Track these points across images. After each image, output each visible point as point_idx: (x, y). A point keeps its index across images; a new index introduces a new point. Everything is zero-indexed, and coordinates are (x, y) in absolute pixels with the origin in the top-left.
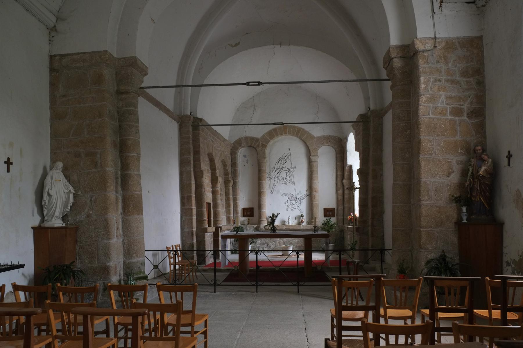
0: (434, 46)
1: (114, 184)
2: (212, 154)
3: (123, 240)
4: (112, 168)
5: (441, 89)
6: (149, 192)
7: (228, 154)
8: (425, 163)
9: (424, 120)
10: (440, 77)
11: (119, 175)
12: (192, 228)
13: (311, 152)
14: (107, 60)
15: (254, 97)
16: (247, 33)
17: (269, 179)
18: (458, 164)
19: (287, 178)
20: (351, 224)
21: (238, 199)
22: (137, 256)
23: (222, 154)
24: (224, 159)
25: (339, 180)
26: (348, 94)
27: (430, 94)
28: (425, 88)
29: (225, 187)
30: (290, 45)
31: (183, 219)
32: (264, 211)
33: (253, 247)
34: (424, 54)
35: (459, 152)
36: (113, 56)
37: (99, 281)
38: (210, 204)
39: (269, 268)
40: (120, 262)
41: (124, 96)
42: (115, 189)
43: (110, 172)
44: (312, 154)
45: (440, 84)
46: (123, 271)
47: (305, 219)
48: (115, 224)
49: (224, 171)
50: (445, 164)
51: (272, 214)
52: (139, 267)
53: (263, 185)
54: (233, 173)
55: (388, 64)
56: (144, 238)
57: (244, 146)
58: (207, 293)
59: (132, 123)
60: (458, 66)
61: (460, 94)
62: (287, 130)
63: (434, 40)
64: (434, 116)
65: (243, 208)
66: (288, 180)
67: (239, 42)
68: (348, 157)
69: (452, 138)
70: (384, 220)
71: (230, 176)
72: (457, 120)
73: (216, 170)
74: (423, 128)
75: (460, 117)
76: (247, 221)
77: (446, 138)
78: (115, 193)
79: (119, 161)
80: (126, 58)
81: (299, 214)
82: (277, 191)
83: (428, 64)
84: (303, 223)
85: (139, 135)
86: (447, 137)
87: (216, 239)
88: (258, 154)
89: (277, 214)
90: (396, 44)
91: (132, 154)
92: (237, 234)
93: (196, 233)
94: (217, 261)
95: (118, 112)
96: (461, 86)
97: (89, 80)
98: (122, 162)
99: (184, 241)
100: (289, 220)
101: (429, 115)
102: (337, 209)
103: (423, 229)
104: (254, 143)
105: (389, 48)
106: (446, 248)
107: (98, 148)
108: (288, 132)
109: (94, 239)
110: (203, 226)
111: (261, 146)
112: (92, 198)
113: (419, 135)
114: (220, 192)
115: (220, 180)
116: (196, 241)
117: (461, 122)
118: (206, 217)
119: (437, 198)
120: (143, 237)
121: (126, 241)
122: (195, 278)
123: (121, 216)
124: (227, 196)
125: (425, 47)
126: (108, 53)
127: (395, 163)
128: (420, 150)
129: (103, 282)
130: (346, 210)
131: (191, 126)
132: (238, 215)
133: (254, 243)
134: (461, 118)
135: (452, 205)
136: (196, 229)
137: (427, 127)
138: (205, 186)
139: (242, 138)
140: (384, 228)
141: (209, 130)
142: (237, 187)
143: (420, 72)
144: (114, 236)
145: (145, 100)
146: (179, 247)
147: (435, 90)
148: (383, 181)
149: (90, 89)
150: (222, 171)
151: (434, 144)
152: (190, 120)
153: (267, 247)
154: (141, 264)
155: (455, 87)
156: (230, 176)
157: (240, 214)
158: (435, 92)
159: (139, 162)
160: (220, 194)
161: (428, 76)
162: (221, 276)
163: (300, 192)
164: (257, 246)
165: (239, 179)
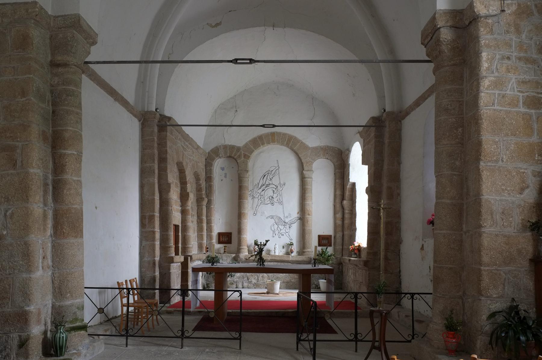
0: (501, 9)
1: (42, 193)
2: (182, 163)
3: (53, 273)
4: (39, 170)
5: (510, 70)
6: (96, 207)
7: (201, 166)
8: (488, 174)
9: (487, 113)
10: (509, 54)
11: (50, 180)
12: (154, 257)
13: (304, 166)
14: (37, 15)
15: (235, 96)
16: (232, 11)
17: (251, 197)
18: (535, 176)
19: (274, 197)
20: (353, 256)
21: (213, 221)
22: (72, 296)
23: (195, 164)
24: (197, 172)
25: (338, 201)
26: (354, 94)
27: (495, 77)
28: (488, 69)
29: (198, 206)
30: (285, 27)
31: (143, 245)
32: (245, 238)
33: (230, 281)
34: (488, 20)
35: (536, 159)
36: (46, 13)
37: (12, 333)
38: (178, 226)
39: (253, 311)
40: (46, 305)
41: (60, 70)
42: (42, 200)
43: (35, 174)
44: (306, 168)
45: (510, 62)
46: (51, 318)
47: (295, 248)
48: (41, 250)
49: (197, 186)
50: (516, 176)
51: (255, 241)
52: (75, 313)
53: (245, 204)
54: (208, 189)
55: (430, 38)
56: (83, 272)
57: (222, 156)
58: (171, 347)
59: (71, 108)
60: (533, 39)
61: (537, 78)
62: (276, 139)
63: (501, 2)
64: (500, 108)
65: (219, 233)
66: (275, 200)
67: (221, 22)
68: (350, 173)
69: (526, 139)
70: (401, 252)
71: (204, 192)
72: (534, 114)
73: (186, 184)
74: (485, 124)
75: (537, 109)
76: (223, 249)
77: (518, 139)
78: (42, 206)
79: (50, 161)
80: (65, 16)
81: (288, 242)
82: (262, 213)
83: (492, 34)
84: (292, 253)
85: (81, 126)
86: (519, 138)
87: (184, 270)
88: (238, 167)
89: (266, 241)
90: (445, 9)
91: (70, 152)
92: (212, 266)
93: (159, 263)
94: (187, 299)
95: (52, 92)
96: (538, 67)
97: (10, 43)
98: (54, 163)
99: (144, 273)
100: (275, 248)
101: (494, 106)
102: (335, 237)
103: (485, 268)
104: (234, 153)
105: (435, 14)
106: (517, 296)
107: (19, 140)
108: (276, 140)
109: (7, 272)
110: (169, 254)
111: (243, 157)
112: (7, 211)
113: (479, 134)
114: (190, 211)
115: (192, 197)
116: (158, 273)
117: (538, 117)
118: (172, 243)
119: (505, 224)
120: (83, 270)
121: (57, 274)
122: (155, 323)
123: (50, 239)
124: (199, 218)
125: (488, 11)
126: (38, 6)
127: (440, 174)
128: (480, 155)
129: (19, 335)
130: (346, 238)
131: (156, 126)
132: (213, 241)
133: (231, 276)
134: (538, 112)
135: (526, 234)
136: (159, 258)
137: (490, 122)
138: (173, 204)
139: (220, 146)
140: (401, 262)
141: (179, 133)
142: (212, 206)
143: (481, 45)
144: (37, 267)
145: (95, 84)
146: (136, 282)
147: (503, 71)
148: (400, 202)
149: (10, 56)
150: (194, 186)
151: (500, 147)
152: (155, 118)
153: (247, 282)
154: (78, 308)
155: (530, 68)
156: (204, 192)
157: (215, 240)
158: (503, 73)
159: (80, 164)
160: (191, 214)
161: (493, 52)
162: (191, 322)
163: (290, 214)
164: (235, 280)
165: (215, 197)
